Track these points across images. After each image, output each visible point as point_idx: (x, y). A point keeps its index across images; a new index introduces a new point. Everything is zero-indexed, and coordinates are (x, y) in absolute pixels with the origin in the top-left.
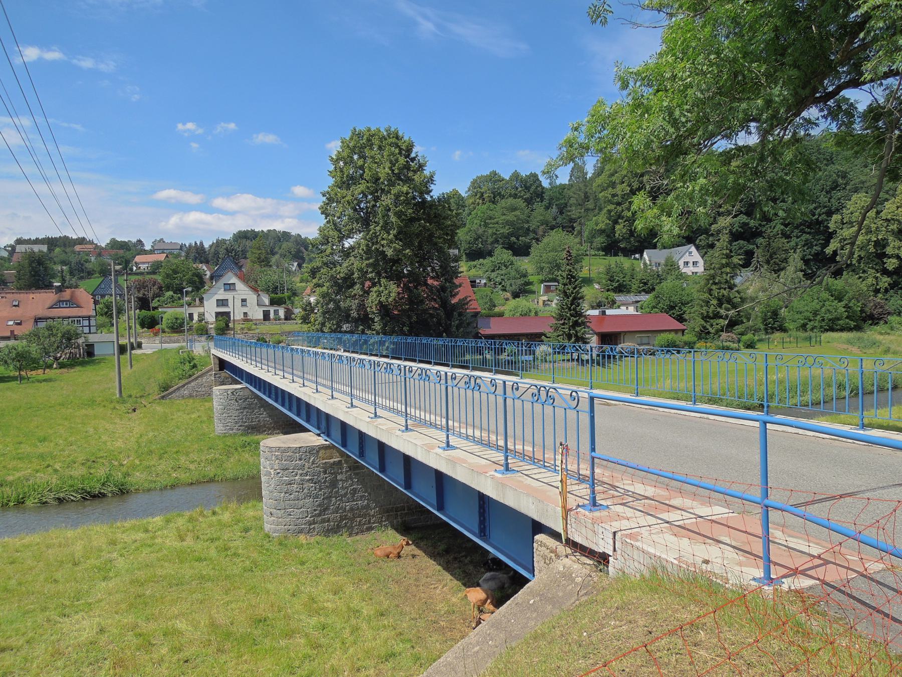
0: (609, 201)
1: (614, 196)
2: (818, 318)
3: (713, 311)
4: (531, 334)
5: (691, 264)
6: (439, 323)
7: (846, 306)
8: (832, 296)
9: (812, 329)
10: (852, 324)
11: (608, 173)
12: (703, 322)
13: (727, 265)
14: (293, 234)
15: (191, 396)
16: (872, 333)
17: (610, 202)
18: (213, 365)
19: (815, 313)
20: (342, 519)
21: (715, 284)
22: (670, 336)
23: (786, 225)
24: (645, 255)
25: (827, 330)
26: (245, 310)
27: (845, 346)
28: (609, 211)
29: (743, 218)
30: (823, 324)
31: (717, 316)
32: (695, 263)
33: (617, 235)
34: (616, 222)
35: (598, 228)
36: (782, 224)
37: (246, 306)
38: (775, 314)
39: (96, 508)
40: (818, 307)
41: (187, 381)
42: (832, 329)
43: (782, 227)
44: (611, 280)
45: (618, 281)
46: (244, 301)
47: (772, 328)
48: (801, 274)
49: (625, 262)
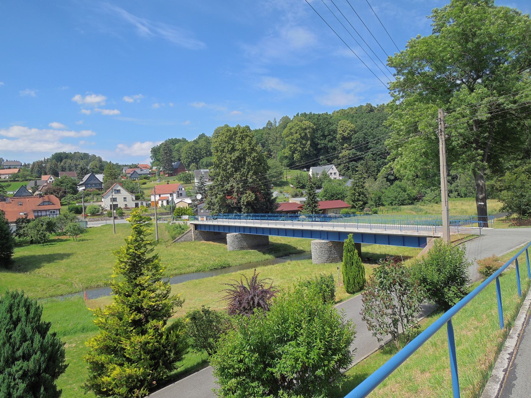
0: (291, 142)
1: (292, 139)
2: (397, 199)
3: (357, 198)
4: (287, 211)
5: (333, 174)
6: (267, 208)
7: (408, 194)
8: (402, 190)
9: (395, 205)
10: (410, 202)
11: (289, 128)
12: (353, 203)
13: (361, 178)
14: (90, 154)
15: (185, 241)
16: (419, 205)
17: (291, 143)
18: (192, 228)
19: (396, 198)
20: (333, 259)
21: (357, 186)
22: (346, 210)
23: (373, 155)
24: (311, 170)
25: (401, 205)
26: (126, 203)
27: (410, 211)
28: (291, 147)
29: (354, 151)
30: (399, 202)
31: (358, 200)
32: (335, 173)
33: (295, 159)
34: (294, 153)
35: (285, 155)
36: (372, 154)
37: (126, 201)
38: (380, 198)
39: (224, 270)
40: (397, 195)
41: (182, 235)
42: (403, 205)
43: (372, 155)
44: (299, 182)
45: (302, 183)
46: (125, 198)
47: (379, 204)
48: (385, 179)
49: (303, 173)
